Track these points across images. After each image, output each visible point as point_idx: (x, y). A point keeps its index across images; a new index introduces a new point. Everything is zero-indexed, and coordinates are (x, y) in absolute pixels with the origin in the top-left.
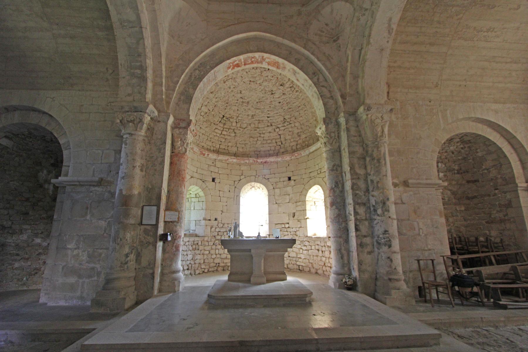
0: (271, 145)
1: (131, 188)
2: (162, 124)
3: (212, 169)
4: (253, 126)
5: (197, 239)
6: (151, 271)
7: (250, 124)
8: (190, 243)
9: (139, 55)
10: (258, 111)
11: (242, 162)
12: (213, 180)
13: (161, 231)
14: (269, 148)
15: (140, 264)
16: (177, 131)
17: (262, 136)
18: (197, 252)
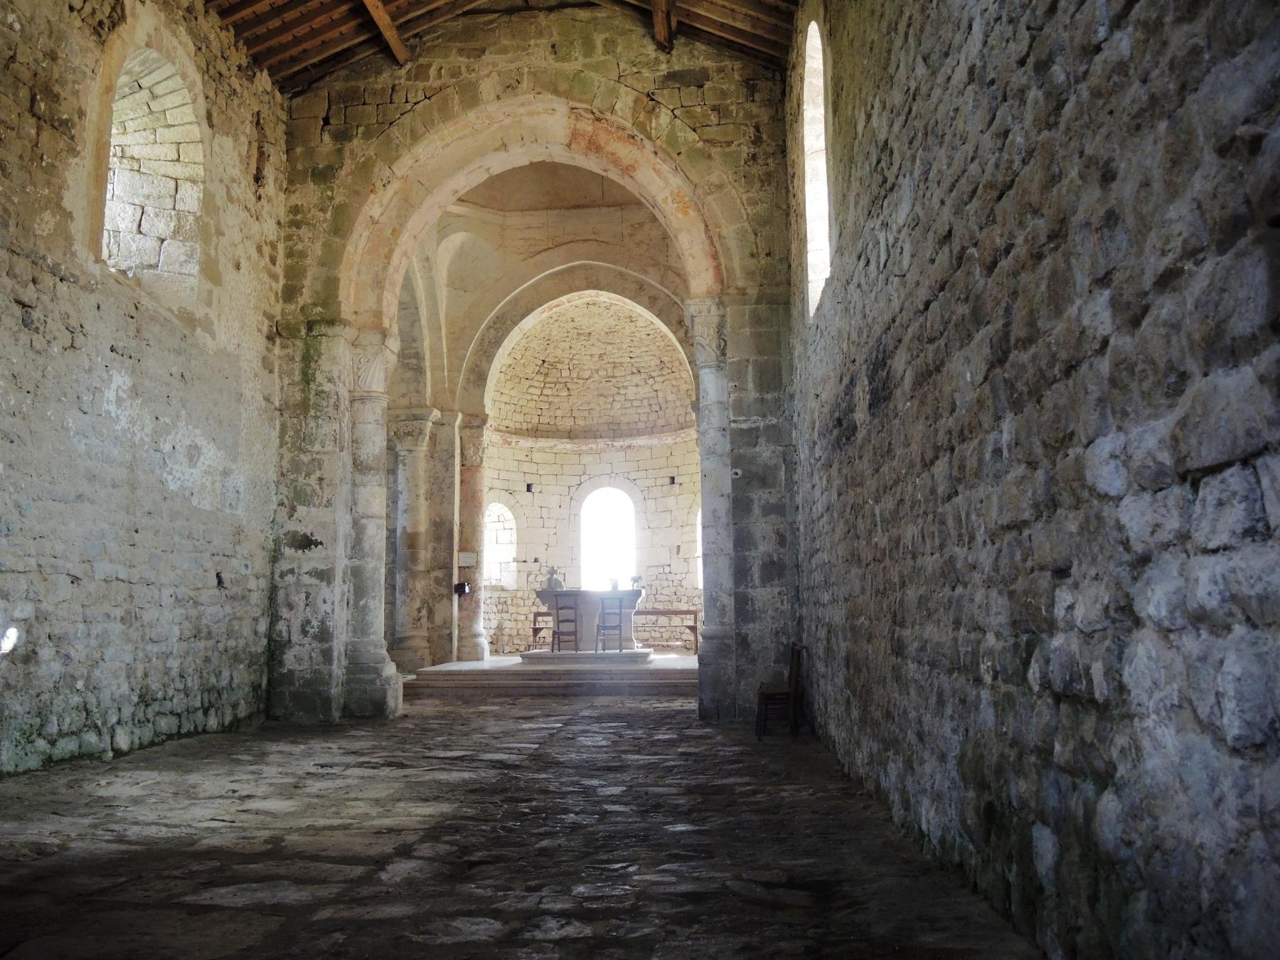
0: (640, 411)
1: (415, 524)
2: (446, 428)
3: (526, 467)
4: (602, 373)
5: (503, 594)
6: (447, 631)
7: (597, 371)
8: (493, 601)
9: (414, 340)
10: (609, 348)
11: (584, 448)
12: (529, 488)
13: (456, 581)
14: (636, 418)
15: (433, 622)
16: (467, 432)
17: (622, 391)
18: (505, 616)
